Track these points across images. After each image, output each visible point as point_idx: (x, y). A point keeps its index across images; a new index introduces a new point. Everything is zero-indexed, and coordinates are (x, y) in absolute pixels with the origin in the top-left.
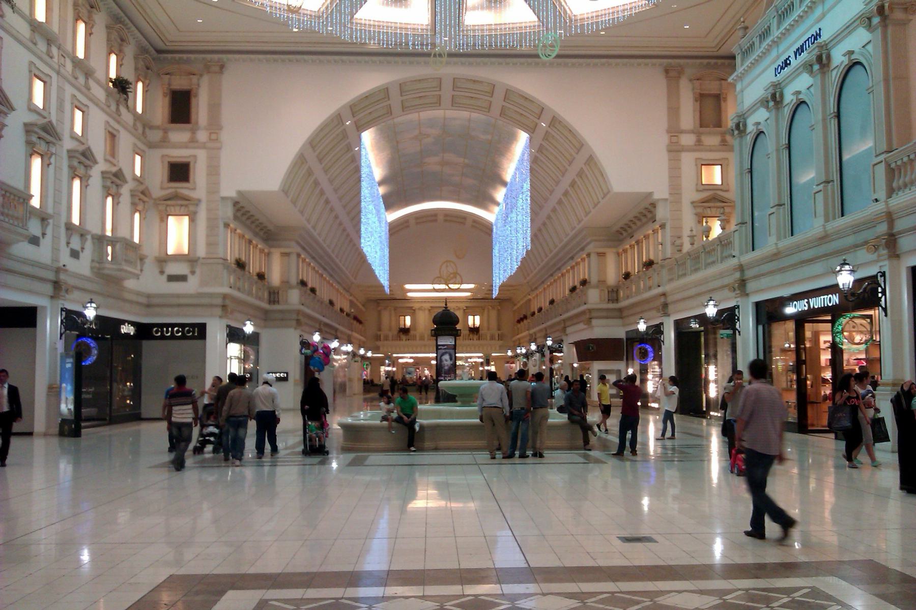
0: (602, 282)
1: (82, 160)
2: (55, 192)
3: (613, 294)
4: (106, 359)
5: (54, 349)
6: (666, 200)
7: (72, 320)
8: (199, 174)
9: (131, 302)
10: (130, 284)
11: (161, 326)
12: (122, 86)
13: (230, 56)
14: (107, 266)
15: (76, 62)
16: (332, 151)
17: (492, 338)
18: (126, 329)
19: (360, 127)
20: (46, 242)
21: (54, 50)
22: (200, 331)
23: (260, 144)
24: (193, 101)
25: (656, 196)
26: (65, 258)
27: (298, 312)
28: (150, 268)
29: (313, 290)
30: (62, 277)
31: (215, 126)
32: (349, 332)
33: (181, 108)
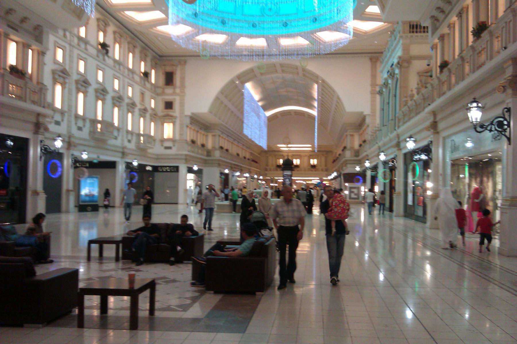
0: (352, 148)
1: (132, 106)
2: (123, 119)
3: (357, 153)
4: (141, 180)
5: (122, 176)
6: (369, 115)
7: (129, 166)
8: (177, 106)
9: (150, 158)
10: (150, 151)
11: (162, 167)
12: (146, 75)
13: (188, 58)
14: (142, 145)
15: (129, 70)
16: (233, 94)
17: (322, 170)
18: (149, 168)
19: (243, 83)
20: (119, 138)
21: (121, 67)
22: (176, 169)
23: (201, 94)
24: (174, 76)
25: (365, 113)
26: (126, 144)
27: (219, 160)
28: (158, 144)
29: (227, 150)
30: (125, 150)
31: (183, 86)
32: (249, 167)
33: (169, 79)
